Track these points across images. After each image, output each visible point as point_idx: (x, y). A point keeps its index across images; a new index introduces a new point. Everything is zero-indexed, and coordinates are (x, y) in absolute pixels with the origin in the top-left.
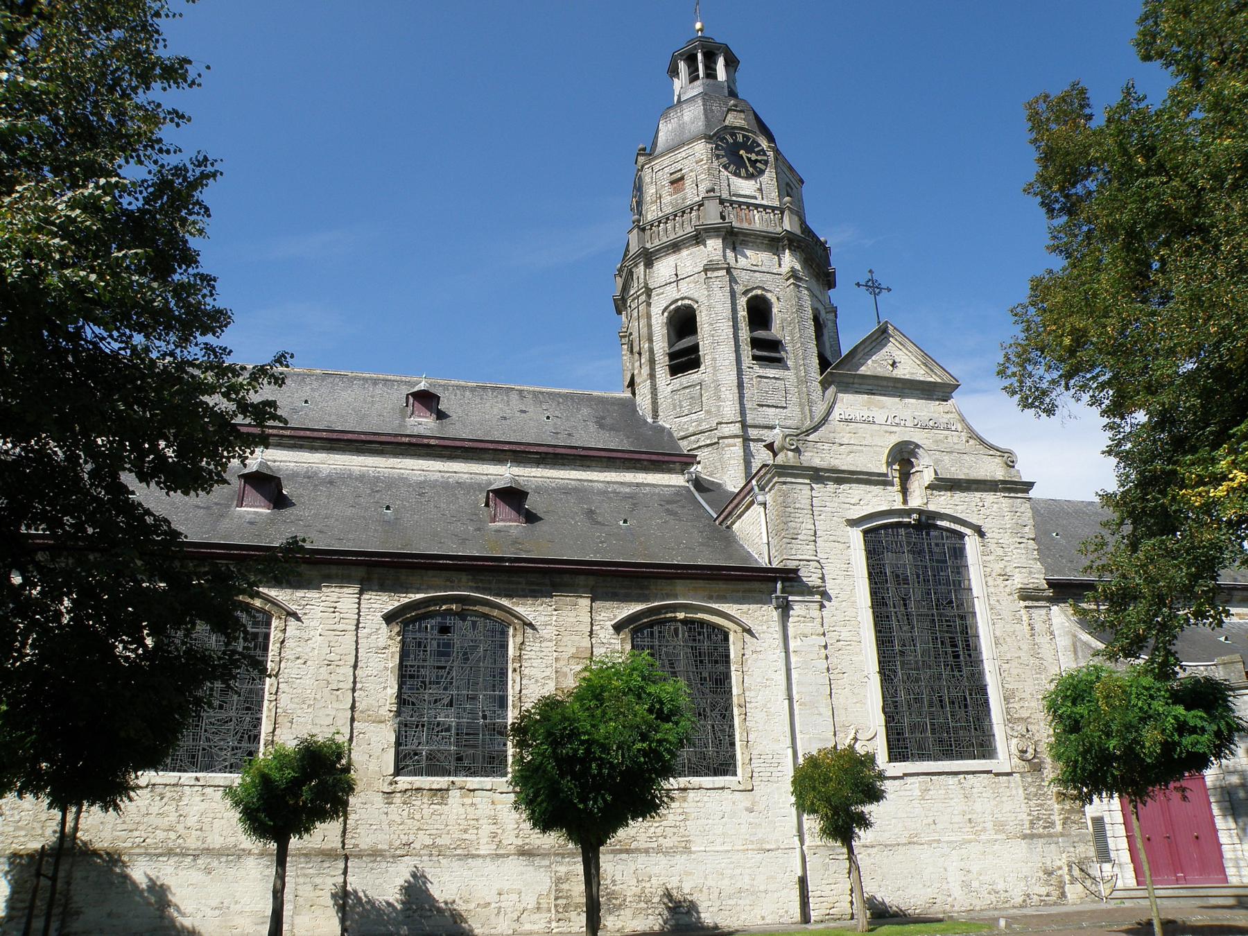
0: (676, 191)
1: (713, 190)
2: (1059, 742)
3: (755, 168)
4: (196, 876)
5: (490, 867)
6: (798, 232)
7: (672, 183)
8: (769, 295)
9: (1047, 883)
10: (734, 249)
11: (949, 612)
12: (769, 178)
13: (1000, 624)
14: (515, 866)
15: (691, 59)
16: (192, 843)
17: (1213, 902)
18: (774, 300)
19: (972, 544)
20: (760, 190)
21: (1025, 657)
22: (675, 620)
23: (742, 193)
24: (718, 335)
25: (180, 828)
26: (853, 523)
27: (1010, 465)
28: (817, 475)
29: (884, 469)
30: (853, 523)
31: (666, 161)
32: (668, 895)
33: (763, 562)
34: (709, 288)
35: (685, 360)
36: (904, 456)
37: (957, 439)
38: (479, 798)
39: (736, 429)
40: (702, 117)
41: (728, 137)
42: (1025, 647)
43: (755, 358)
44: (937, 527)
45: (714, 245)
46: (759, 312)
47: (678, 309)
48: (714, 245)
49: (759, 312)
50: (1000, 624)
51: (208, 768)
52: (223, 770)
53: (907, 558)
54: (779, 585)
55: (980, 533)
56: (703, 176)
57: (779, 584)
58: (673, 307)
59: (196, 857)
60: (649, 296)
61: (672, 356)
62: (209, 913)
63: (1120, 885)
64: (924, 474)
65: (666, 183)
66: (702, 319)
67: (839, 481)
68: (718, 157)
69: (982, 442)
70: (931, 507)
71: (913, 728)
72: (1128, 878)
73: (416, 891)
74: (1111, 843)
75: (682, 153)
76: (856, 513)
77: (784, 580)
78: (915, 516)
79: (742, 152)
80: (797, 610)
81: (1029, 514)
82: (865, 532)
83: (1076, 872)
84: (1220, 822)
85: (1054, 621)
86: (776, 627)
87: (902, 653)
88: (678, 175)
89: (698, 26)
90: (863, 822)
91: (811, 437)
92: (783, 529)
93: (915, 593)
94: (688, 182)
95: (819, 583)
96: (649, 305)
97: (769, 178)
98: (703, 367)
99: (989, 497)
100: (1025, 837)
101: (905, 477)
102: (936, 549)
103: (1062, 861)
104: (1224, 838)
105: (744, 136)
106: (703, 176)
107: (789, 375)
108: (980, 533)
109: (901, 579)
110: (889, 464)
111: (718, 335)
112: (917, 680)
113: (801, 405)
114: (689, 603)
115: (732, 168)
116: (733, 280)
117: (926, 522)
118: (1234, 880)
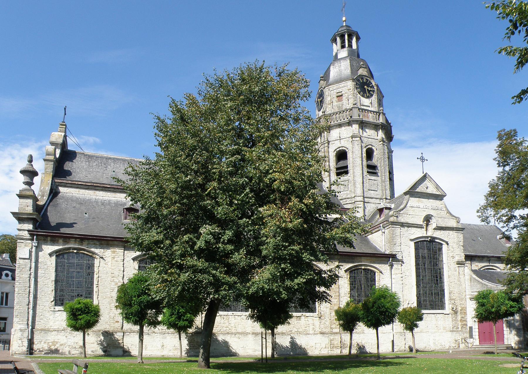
0: (339, 101)
1: (356, 104)
2: (478, 308)
3: (370, 93)
4: (235, 339)
5: (313, 337)
6: (385, 122)
7: (337, 97)
8: (373, 148)
9: (455, 343)
10: (362, 129)
11: (436, 267)
12: (374, 98)
13: (450, 271)
14: (319, 336)
15: (342, 36)
16: (233, 331)
17: (500, 348)
18: (375, 150)
19: (445, 247)
20: (371, 103)
21: (456, 281)
22: (361, 269)
23: (365, 104)
24: (356, 161)
25: (230, 327)
26: (411, 240)
27: (458, 222)
28: (403, 225)
29: (422, 223)
30: (411, 240)
31: (335, 87)
32: (358, 344)
33: (387, 253)
34: (353, 144)
35: (342, 171)
36: (428, 219)
37: (444, 213)
38: (309, 318)
39: (361, 199)
40: (350, 68)
41: (360, 79)
42: (456, 278)
43: (368, 172)
44: (435, 242)
45: (356, 127)
46: (370, 154)
47: (340, 150)
48: (356, 127)
49: (370, 154)
50: (450, 271)
51: (235, 310)
52: (239, 311)
53: (426, 251)
54: (391, 259)
55: (447, 243)
56: (351, 96)
57: (389, 258)
58: (338, 150)
59: (235, 334)
60: (329, 144)
61: (337, 169)
62: (241, 349)
63: (475, 344)
64: (433, 224)
65: (335, 96)
66: (349, 155)
67: (408, 227)
68: (357, 88)
69: (451, 214)
70: (434, 236)
71: (424, 301)
72: (477, 342)
73: (293, 343)
74: (474, 334)
75: (342, 84)
76: (413, 237)
77: (392, 257)
78: (430, 238)
79: (365, 87)
80: (395, 266)
81: (462, 238)
82: (415, 243)
83: (463, 341)
84: (505, 329)
85: (465, 271)
86: (389, 271)
87: (422, 279)
88: (340, 94)
89: (344, 19)
90: (416, 326)
91: (401, 212)
92: (391, 241)
93: (427, 262)
94: (344, 98)
95: (401, 258)
96: (329, 147)
97: (374, 98)
98: (349, 174)
99: (451, 232)
100: (451, 331)
101: (427, 225)
102: (434, 249)
103: (460, 338)
104: (505, 332)
105: (366, 79)
106: (351, 96)
107: (379, 179)
108: (447, 243)
109: (424, 257)
110: (423, 222)
111: (356, 161)
112: (426, 287)
113: (382, 190)
114: (365, 264)
115: (362, 93)
116: (362, 142)
117: (433, 240)
118: (506, 343)
